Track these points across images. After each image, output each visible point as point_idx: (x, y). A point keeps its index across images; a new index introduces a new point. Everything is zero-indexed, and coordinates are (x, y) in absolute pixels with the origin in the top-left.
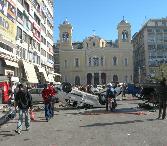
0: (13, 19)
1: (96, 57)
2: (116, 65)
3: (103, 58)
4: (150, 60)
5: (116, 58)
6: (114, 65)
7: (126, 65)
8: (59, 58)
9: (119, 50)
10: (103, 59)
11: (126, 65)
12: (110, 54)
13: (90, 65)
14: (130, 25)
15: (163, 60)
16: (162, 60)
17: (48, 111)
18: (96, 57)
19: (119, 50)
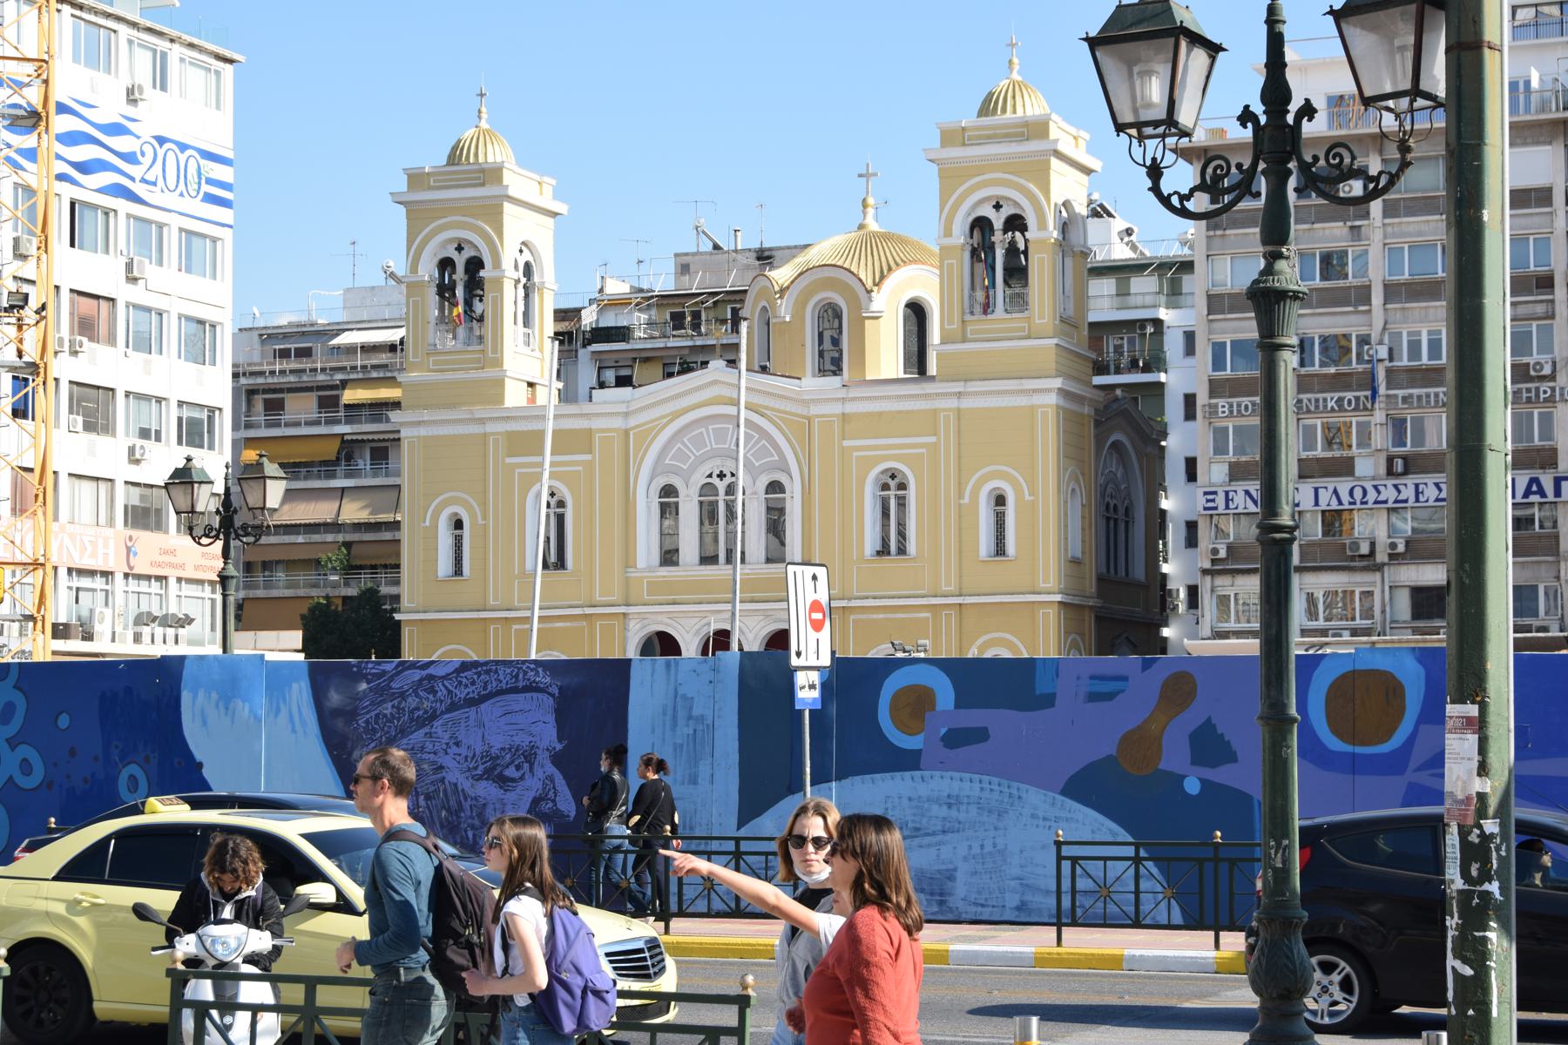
0: (974, 387)
1: (721, 476)
2: (902, 551)
3: (783, 479)
4: (1408, 493)
5: (902, 486)
6: (884, 551)
7: (1000, 550)
8: (662, 504)
9: (1022, 401)
10: (783, 491)
11: (1000, 550)
12: (846, 443)
13: (669, 557)
14: (1052, 136)
15: (1358, 493)
16: (1345, 498)
17: (432, 987)
18: (721, 476)
19: (1022, 401)
